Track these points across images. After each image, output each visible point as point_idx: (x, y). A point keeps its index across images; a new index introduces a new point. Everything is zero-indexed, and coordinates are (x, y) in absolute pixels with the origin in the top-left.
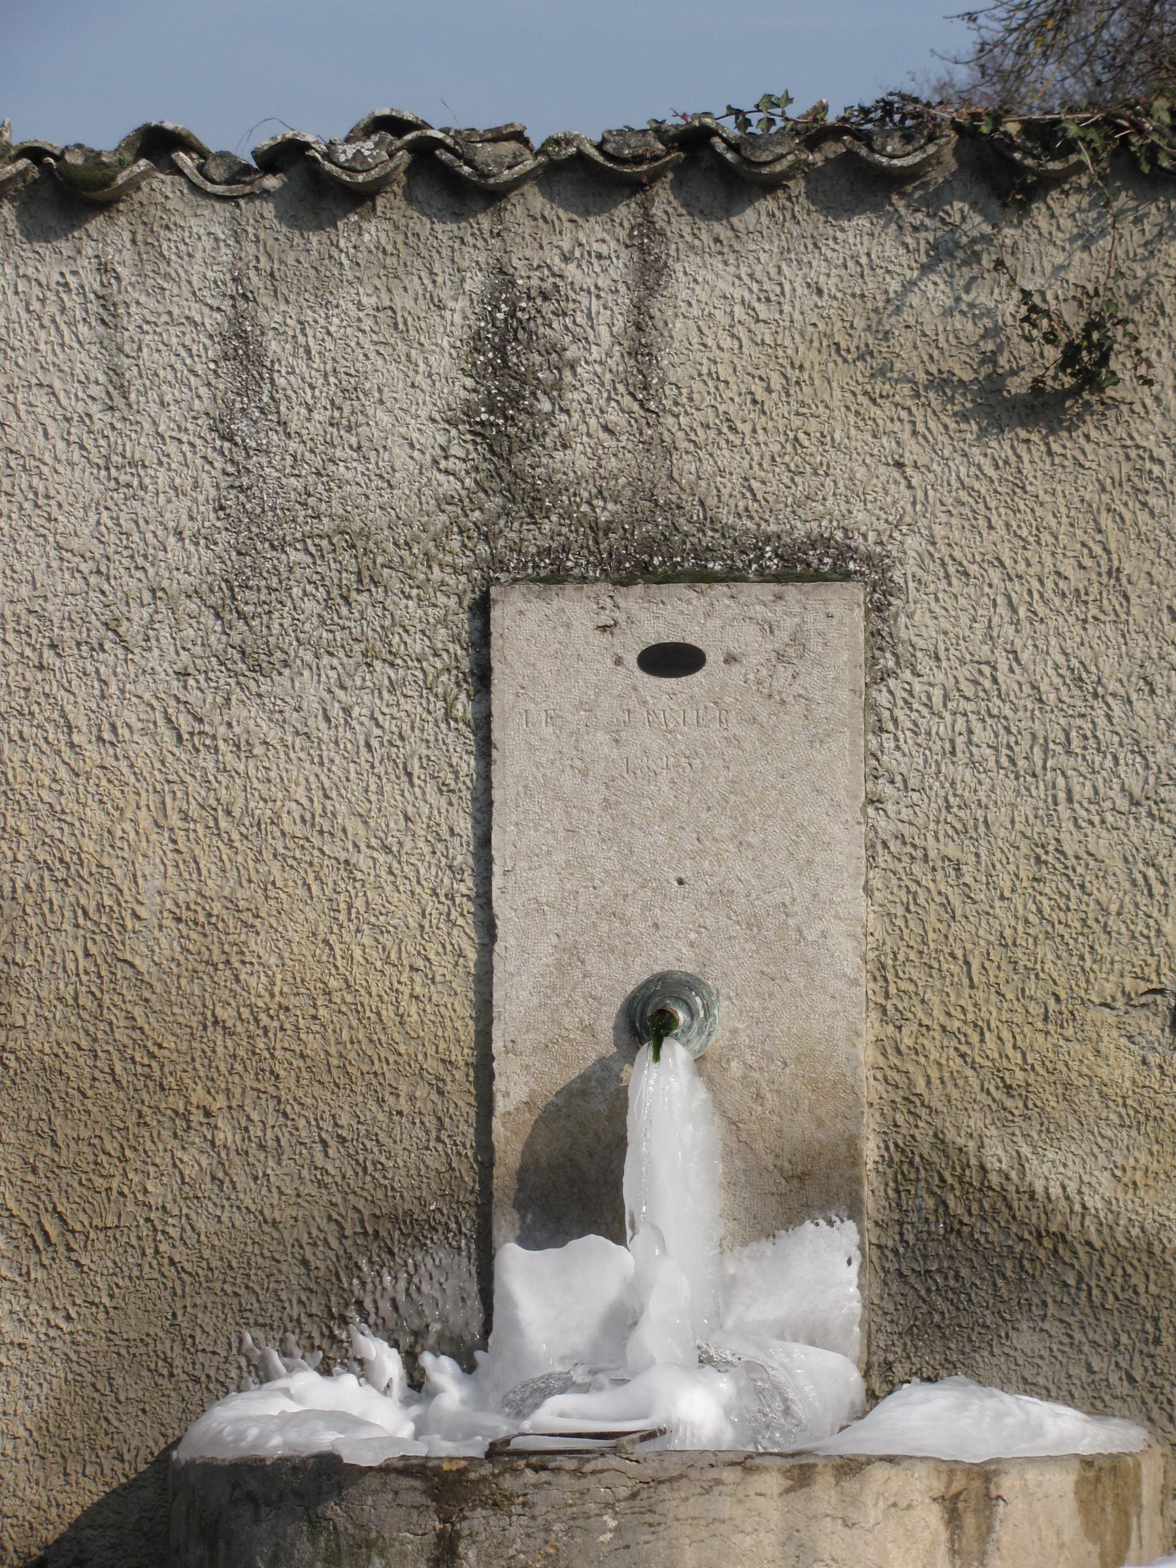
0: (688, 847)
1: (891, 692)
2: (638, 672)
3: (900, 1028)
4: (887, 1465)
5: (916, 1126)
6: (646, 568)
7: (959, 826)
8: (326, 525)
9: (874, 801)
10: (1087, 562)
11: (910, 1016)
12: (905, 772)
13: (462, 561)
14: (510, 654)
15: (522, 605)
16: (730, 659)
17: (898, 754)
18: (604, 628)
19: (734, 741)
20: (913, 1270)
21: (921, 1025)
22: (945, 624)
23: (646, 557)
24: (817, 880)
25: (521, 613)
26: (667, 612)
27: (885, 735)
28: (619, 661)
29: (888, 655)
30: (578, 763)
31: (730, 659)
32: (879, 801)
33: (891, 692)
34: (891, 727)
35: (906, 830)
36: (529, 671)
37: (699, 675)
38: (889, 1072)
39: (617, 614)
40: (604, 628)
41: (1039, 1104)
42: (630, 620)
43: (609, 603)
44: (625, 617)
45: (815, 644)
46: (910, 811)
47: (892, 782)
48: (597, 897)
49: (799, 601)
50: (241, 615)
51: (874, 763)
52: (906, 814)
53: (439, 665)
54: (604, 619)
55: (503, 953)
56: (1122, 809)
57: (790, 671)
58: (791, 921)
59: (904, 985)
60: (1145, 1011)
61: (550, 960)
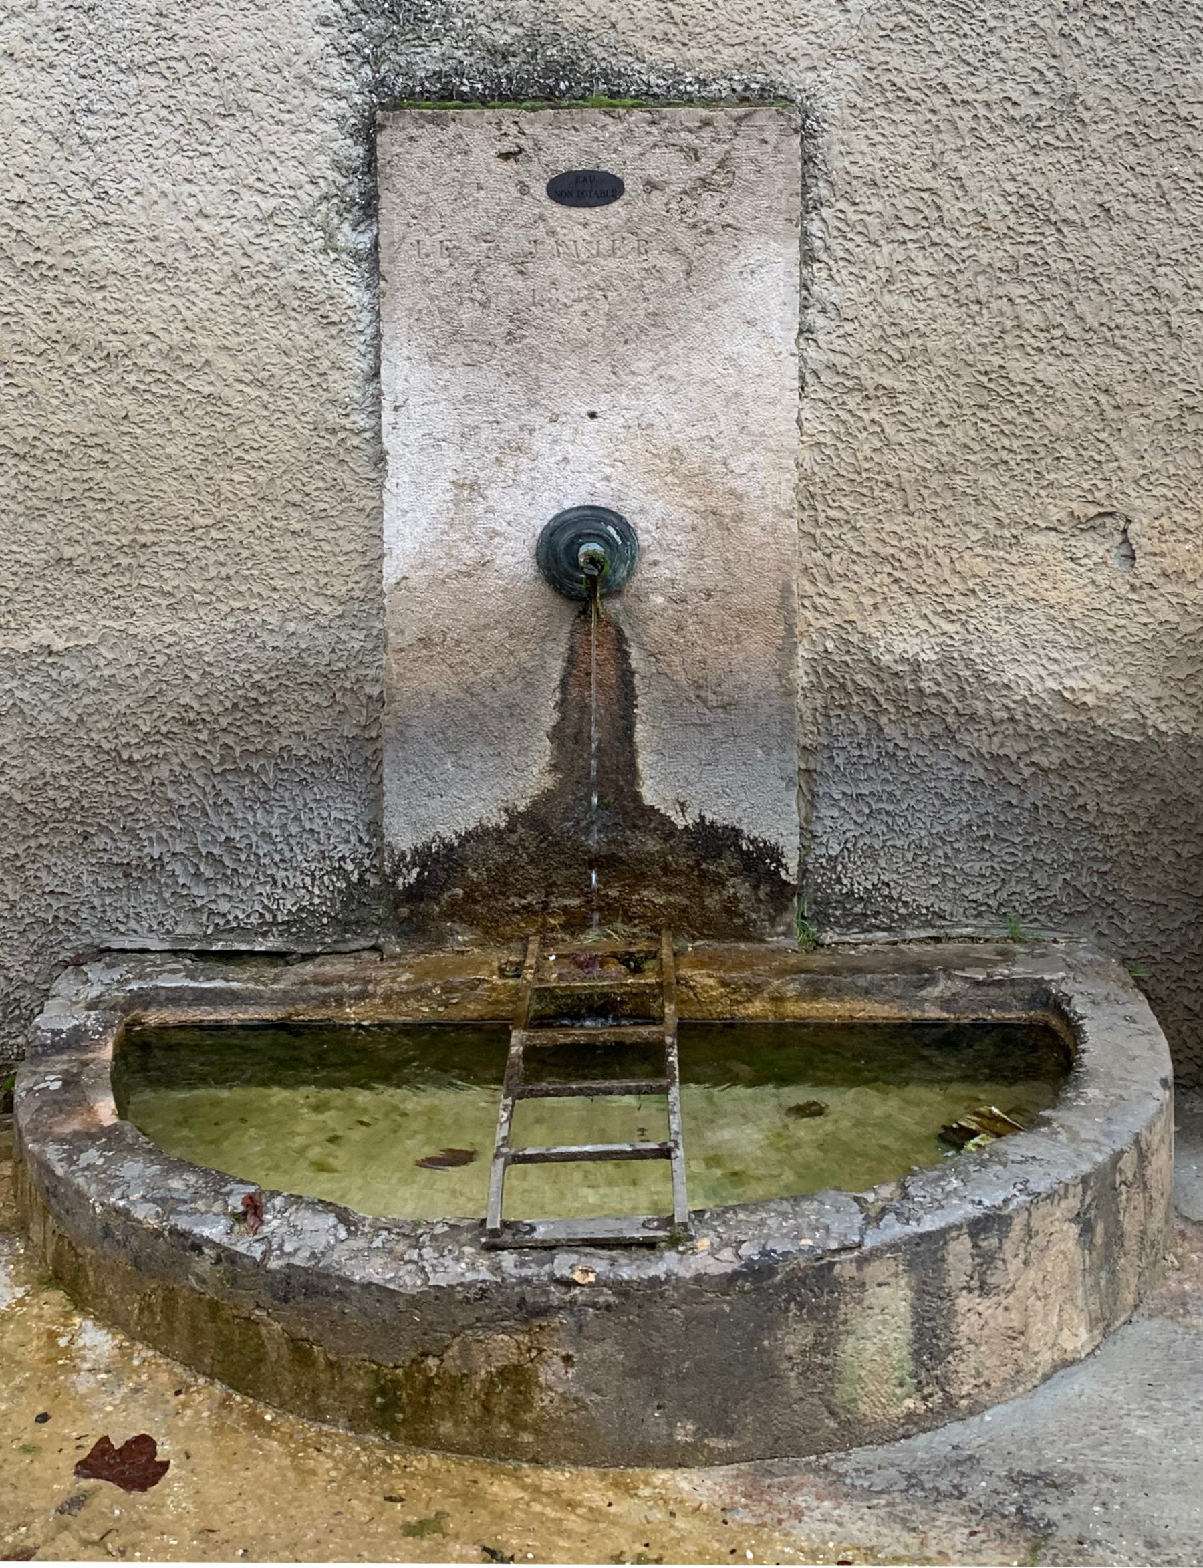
0: (603, 381)
1: (824, 220)
2: (548, 202)
3: (829, 556)
4: (645, 1252)
5: (848, 652)
6: (552, 93)
7: (897, 356)
8: (182, 47)
9: (806, 331)
10: (1039, 87)
11: (841, 544)
12: (837, 302)
13: (341, 86)
14: (400, 184)
15: (414, 132)
16: (651, 186)
17: (829, 284)
18: (505, 156)
19: (654, 271)
20: (844, 794)
21: (852, 551)
22: (883, 152)
23: (551, 82)
24: (747, 413)
25: (411, 139)
26: (580, 138)
27: (816, 266)
28: (524, 189)
29: (821, 184)
30: (479, 296)
31: (651, 186)
32: (810, 331)
33: (824, 220)
34: (824, 257)
35: (836, 359)
36: (421, 200)
37: (615, 205)
38: (818, 600)
39: (522, 141)
40: (505, 156)
41: (981, 628)
42: (538, 147)
43: (513, 130)
44: (531, 144)
45: (746, 170)
46: (842, 341)
47: (824, 311)
48: (501, 431)
49: (730, 128)
50: (85, 141)
51: (805, 293)
52: (839, 344)
53: (317, 194)
54: (507, 146)
55: (395, 490)
56: (1075, 336)
57: (717, 201)
58: (717, 455)
59: (832, 513)
60: (1092, 533)
61: (449, 496)
